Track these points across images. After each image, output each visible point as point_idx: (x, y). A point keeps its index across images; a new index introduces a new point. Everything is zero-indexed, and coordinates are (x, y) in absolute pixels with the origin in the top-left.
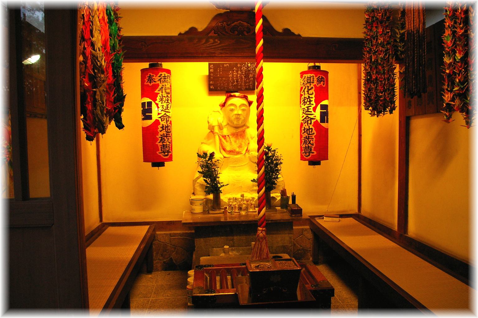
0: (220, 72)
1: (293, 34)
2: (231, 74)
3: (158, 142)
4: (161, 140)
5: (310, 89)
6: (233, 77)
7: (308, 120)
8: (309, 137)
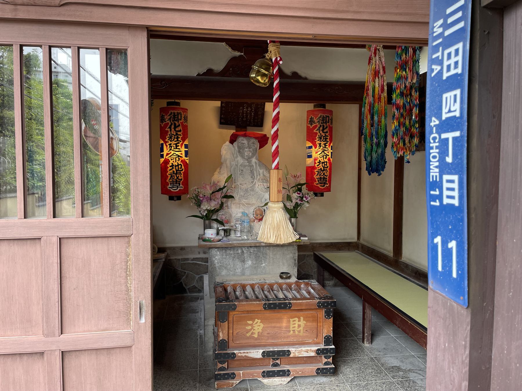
1: (300, 77)
3: (168, 179)
4: (171, 177)
6: (243, 113)
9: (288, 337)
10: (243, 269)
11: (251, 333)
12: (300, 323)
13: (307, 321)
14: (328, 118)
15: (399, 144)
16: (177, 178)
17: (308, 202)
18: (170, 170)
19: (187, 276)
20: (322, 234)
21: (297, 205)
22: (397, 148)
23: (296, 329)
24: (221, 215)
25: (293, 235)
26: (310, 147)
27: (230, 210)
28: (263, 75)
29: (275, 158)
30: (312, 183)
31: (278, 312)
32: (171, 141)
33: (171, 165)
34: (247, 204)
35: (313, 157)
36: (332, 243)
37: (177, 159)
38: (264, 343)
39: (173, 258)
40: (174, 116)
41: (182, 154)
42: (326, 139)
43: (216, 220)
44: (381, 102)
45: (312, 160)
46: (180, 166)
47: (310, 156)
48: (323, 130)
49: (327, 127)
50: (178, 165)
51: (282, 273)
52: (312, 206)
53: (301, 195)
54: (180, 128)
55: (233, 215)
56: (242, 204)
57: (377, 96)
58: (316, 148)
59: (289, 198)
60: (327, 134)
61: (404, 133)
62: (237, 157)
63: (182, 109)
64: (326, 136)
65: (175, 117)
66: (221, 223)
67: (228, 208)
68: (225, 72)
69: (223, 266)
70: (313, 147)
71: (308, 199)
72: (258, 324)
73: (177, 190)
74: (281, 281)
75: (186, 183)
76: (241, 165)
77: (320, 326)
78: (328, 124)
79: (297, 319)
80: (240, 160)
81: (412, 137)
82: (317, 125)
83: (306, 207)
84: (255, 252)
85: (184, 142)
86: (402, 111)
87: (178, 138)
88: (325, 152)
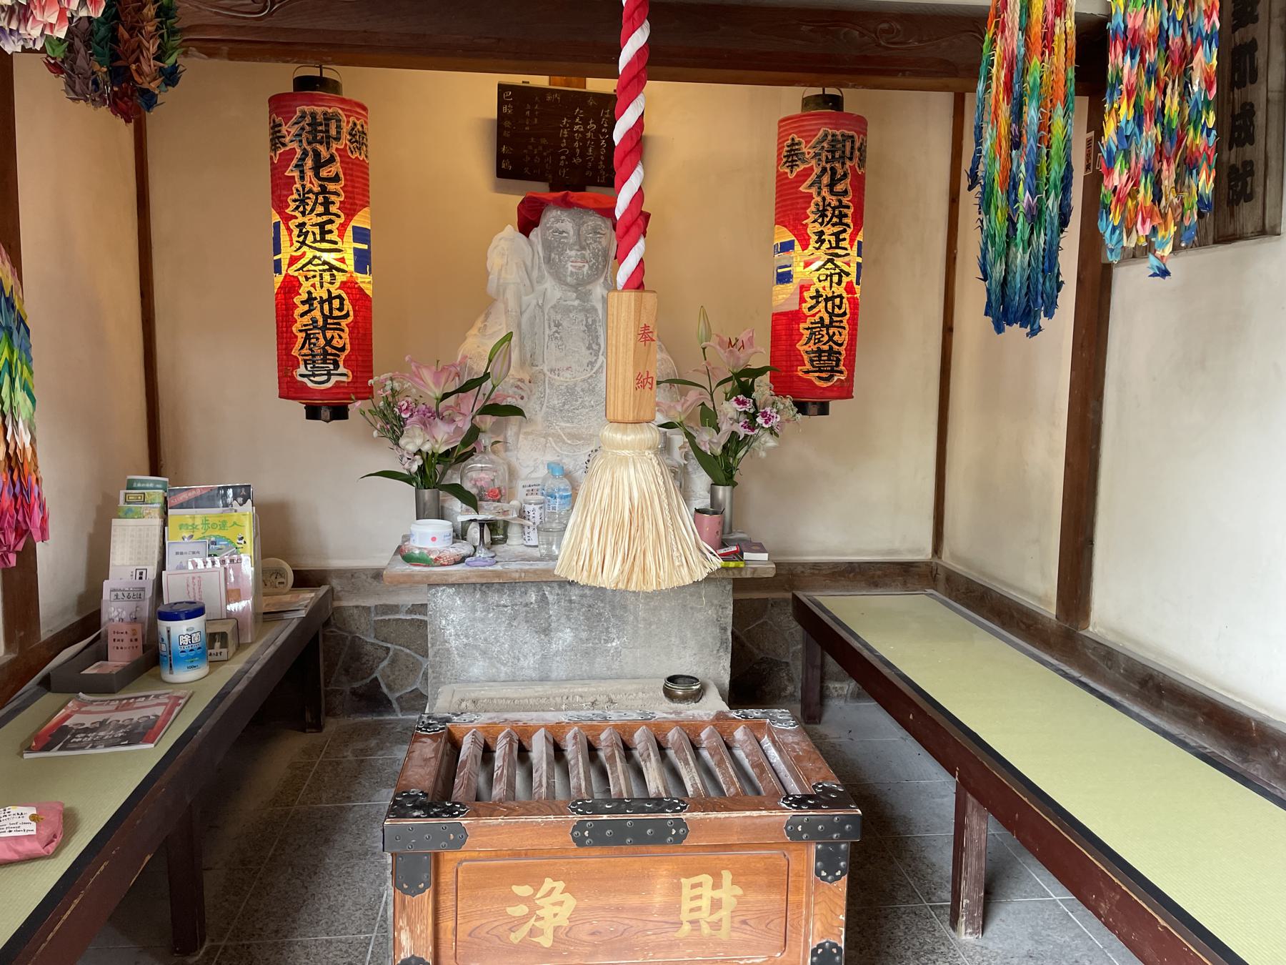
2: (565, 127)
4: (308, 337)
5: (840, 180)
6: (571, 139)
7: (831, 275)
8: (832, 321)
9: (672, 945)
10: (544, 657)
11: (526, 929)
12: (717, 894)
13: (746, 886)
14: (848, 145)
15: (1133, 194)
16: (329, 342)
17: (772, 431)
18: (302, 315)
19: (393, 662)
20: (826, 535)
21: (734, 444)
22: (1122, 213)
23: (704, 915)
24: (476, 474)
25: (696, 554)
27: (512, 457)
29: (628, 239)
30: (791, 368)
31: (634, 854)
32: (303, 213)
33: (305, 296)
35: (796, 280)
36: (851, 563)
37: (327, 277)
39: (348, 602)
40: (314, 124)
41: (342, 260)
42: (842, 216)
43: (458, 491)
44: (1052, 50)
46: (336, 303)
47: (784, 278)
48: (831, 186)
49: (845, 175)
50: (330, 299)
51: (672, 679)
52: (787, 442)
53: (749, 407)
54: (336, 168)
55: (523, 472)
56: (553, 435)
57: (1037, 29)
58: (805, 247)
59: (709, 417)
60: (845, 201)
61: (1160, 153)
62: (541, 279)
63: (344, 101)
64: (841, 205)
65: (318, 131)
66: (471, 501)
67: (506, 450)
69: (476, 647)
70: (797, 247)
71: (774, 422)
72: (557, 896)
73: (329, 385)
74: (664, 710)
75: (362, 360)
76: (554, 307)
77: (799, 906)
78: (848, 163)
79: (706, 879)
80: (553, 290)
81: (1189, 165)
82: (811, 169)
83: (768, 451)
84: (585, 601)
85: (350, 215)
86: (1151, 56)
87: (327, 203)
88: (838, 262)
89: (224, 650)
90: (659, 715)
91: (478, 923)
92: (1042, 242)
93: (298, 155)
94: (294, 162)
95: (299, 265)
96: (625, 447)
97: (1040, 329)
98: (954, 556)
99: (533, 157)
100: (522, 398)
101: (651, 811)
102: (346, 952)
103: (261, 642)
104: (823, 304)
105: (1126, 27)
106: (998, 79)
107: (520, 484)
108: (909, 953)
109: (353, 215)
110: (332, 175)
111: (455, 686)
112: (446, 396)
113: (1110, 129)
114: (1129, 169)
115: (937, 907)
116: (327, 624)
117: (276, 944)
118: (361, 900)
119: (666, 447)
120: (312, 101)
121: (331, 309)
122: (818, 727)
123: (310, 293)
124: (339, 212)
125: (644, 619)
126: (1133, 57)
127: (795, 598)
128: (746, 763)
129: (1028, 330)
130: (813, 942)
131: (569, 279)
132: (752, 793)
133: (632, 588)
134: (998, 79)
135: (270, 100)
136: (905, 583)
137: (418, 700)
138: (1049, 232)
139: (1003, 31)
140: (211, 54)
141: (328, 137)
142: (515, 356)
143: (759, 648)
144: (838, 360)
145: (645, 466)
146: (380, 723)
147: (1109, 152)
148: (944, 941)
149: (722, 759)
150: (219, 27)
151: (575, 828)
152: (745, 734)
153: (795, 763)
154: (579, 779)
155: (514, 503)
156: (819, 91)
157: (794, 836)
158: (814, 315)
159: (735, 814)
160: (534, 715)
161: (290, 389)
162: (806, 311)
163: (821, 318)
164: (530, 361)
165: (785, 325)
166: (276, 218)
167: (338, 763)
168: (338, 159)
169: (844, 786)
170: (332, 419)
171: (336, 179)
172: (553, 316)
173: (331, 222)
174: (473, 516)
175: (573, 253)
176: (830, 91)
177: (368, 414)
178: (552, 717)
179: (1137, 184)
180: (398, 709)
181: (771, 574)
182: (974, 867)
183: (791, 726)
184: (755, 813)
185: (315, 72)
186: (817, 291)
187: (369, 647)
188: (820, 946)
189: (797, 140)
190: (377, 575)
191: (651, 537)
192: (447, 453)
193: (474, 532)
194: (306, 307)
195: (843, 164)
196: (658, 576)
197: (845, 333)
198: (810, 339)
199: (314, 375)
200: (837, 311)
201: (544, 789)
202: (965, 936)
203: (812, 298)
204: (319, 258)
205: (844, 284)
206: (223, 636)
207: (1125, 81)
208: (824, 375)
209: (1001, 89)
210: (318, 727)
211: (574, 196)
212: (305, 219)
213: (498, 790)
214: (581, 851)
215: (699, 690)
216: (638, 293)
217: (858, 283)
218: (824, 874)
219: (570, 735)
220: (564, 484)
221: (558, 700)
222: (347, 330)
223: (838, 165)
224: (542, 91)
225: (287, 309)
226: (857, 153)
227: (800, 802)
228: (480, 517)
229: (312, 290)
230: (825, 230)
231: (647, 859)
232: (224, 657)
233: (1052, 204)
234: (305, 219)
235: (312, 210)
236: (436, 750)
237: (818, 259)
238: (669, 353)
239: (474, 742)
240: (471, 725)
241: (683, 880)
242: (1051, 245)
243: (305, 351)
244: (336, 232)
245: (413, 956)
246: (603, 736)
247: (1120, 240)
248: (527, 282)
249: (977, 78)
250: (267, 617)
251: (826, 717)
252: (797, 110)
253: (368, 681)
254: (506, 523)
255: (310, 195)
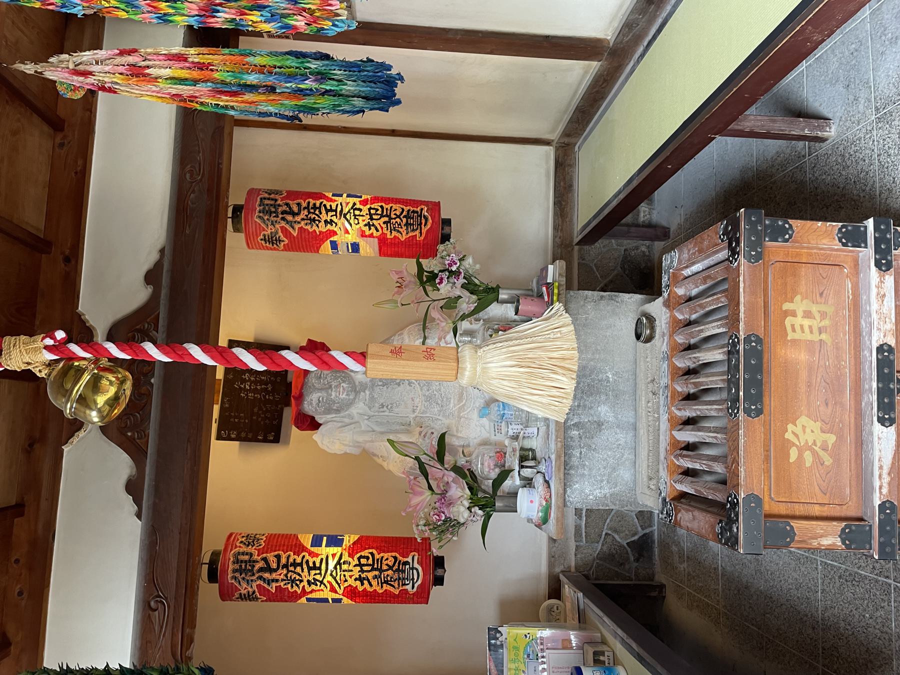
0: (240, 418)
1: (158, 265)
2: (247, 395)
4: (386, 582)
5: (290, 208)
6: (255, 391)
7: (355, 215)
8: (387, 216)
11: (822, 453)
12: (800, 313)
13: (795, 292)
14: (266, 202)
16: (390, 568)
18: (371, 585)
19: (615, 531)
20: (534, 221)
21: (470, 286)
22: (324, 19)
23: (815, 324)
24: (486, 469)
26: (334, 246)
27: (474, 442)
28: (95, 385)
30: (418, 244)
31: (769, 374)
32: (301, 581)
33: (358, 583)
34: (460, 399)
37: (345, 567)
38: (853, 415)
40: (240, 571)
41: (334, 555)
42: (314, 207)
43: (498, 482)
45: (362, 243)
46: (363, 561)
47: (355, 248)
48: (294, 214)
49: (287, 204)
50: (360, 565)
51: (638, 337)
52: (468, 249)
53: (445, 275)
55: (485, 435)
56: (459, 412)
57: (196, 74)
58: (335, 233)
59: (451, 303)
60: (304, 205)
62: (350, 416)
64: (307, 208)
65: (245, 568)
66: (505, 474)
67: (468, 446)
68: (136, 451)
69: (610, 475)
71: (456, 259)
72: (799, 430)
74: (661, 344)
75: (403, 545)
76: (370, 408)
77: (810, 255)
78: (279, 202)
79: (788, 321)
80: (359, 408)
82: (282, 228)
83: (475, 262)
85: (304, 549)
87: (295, 564)
88: (346, 210)
89: (606, 654)
90: (665, 348)
91: (817, 488)
92: (339, 72)
93: (262, 583)
94: (266, 585)
95: (336, 586)
96: (475, 369)
97: (399, 74)
98: (553, 131)
99: (266, 418)
100: (432, 433)
101: (738, 360)
102: (831, 579)
103: (601, 627)
104: (374, 221)
105: (197, 15)
106: (227, 101)
107: (493, 438)
108: (844, 173)
109: (303, 546)
110: (275, 560)
111: (638, 492)
112: (430, 488)
113: (266, 27)
114: (294, 14)
115: (809, 151)
116: (587, 577)
117: (823, 630)
118: (792, 566)
119: (470, 333)
120: (224, 571)
121: (367, 565)
122: (672, 230)
123: (356, 579)
124: (301, 556)
125: (593, 354)
126: (218, 11)
127: (578, 244)
128: (702, 288)
129: (399, 82)
130: (838, 245)
131: (351, 397)
132: (724, 284)
133: (576, 368)
134: (227, 101)
135: (223, 600)
136: (570, 165)
137: (645, 516)
138: (333, 68)
139: (196, 97)
140: (191, 641)
141: (250, 561)
142: (404, 438)
143: (613, 270)
144: (413, 212)
145: (489, 355)
146: (660, 542)
147: (281, 28)
148: (835, 147)
149: (698, 305)
150: (173, 635)
151: (749, 416)
152: (680, 287)
153: (703, 253)
154: (711, 409)
155: (507, 442)
156: (230, 221)
157: (759, 257)
158: (382, 228)
159: (742, 300)
160: (661, 437)
161: (422, 596)
162: (379, 234)
163: (384, 223)
164: (407, 427)
165: (387, 247)
166: (303, 600)
167: (689, 574)
168: (264, 555)
169: (721, 220)
170: (444, 568)
171: (278, 557)
172: (376, 409)
173: (307, 562)
174: (516, 473)
175: (333, 394)
176: (230, 210)
177: (441, 544)
178: (664, 425)
179: (304, 10)
180: (650, 529)
181: (563, 263)
182: (782, 125)
183: (675, 254)
184: (742, 285)
185: (205, 568)
186: (365, 225)
187: (605, 548)
188: (840, 240)
189: (262, 237)
190: (552, 540)
191: (539, 353)
192: (470, 488)
193: (527, 472)
194: (366, 582)
195: (279, 205)
196: (568, 350)
197: (395, 207)
198: (398, 231)
199: (413, 579)
200: (379, 212)
201: (719, 436)
202: (832, 132)
203: (370, 229)
204: (332, 572)
205: (361, 207)
206: (595, 653)
207: (234, 17)
208: (423, 221)
209: (234, 99)
210: (662, 587)
211: (294, 392)
212: (305, 580)
213: (719, 468)
214: (766, 411)
215: (647, 318)
216: (369, 356)
217: (361, 197)
218: (787, 236)
219: (678, 413)
220: (494, 407)
221: (651, 418)
222: (382, 555)
223: (280, 209)
224: (222, 410)
225: (367, 596)
226: (272, 196)
227: (734, 252)
228: (517, 468)
229: (353, 578)
230: (324, 219)
231: (773, 363)
232: (611, 654)
233: (314, 65)
234: (305, 580)
235: (299, 575)
236: (687, 511)
237: (343, 224)
238: (403, 329)
239: (681, 482)
240: (668, 484)
241: (789, 338)
242: (342, 66)
243: (396, 585)
244: (315, 559)
245: (840, 536)
246: (679, 389)
247: (342, 21)
248: (353, 426)
249: (224, 115)
250: (582, 621)
251: (664, 223)
252: (242, 236)
253: (629, 549)
254: (522, 449)
255: (289, 575)
